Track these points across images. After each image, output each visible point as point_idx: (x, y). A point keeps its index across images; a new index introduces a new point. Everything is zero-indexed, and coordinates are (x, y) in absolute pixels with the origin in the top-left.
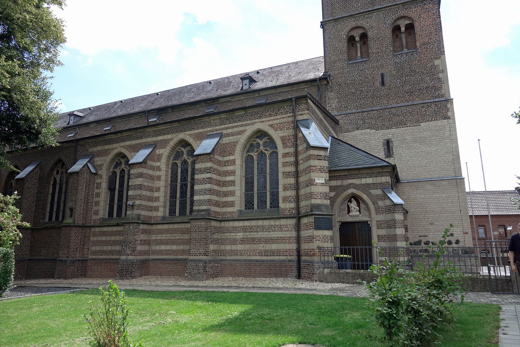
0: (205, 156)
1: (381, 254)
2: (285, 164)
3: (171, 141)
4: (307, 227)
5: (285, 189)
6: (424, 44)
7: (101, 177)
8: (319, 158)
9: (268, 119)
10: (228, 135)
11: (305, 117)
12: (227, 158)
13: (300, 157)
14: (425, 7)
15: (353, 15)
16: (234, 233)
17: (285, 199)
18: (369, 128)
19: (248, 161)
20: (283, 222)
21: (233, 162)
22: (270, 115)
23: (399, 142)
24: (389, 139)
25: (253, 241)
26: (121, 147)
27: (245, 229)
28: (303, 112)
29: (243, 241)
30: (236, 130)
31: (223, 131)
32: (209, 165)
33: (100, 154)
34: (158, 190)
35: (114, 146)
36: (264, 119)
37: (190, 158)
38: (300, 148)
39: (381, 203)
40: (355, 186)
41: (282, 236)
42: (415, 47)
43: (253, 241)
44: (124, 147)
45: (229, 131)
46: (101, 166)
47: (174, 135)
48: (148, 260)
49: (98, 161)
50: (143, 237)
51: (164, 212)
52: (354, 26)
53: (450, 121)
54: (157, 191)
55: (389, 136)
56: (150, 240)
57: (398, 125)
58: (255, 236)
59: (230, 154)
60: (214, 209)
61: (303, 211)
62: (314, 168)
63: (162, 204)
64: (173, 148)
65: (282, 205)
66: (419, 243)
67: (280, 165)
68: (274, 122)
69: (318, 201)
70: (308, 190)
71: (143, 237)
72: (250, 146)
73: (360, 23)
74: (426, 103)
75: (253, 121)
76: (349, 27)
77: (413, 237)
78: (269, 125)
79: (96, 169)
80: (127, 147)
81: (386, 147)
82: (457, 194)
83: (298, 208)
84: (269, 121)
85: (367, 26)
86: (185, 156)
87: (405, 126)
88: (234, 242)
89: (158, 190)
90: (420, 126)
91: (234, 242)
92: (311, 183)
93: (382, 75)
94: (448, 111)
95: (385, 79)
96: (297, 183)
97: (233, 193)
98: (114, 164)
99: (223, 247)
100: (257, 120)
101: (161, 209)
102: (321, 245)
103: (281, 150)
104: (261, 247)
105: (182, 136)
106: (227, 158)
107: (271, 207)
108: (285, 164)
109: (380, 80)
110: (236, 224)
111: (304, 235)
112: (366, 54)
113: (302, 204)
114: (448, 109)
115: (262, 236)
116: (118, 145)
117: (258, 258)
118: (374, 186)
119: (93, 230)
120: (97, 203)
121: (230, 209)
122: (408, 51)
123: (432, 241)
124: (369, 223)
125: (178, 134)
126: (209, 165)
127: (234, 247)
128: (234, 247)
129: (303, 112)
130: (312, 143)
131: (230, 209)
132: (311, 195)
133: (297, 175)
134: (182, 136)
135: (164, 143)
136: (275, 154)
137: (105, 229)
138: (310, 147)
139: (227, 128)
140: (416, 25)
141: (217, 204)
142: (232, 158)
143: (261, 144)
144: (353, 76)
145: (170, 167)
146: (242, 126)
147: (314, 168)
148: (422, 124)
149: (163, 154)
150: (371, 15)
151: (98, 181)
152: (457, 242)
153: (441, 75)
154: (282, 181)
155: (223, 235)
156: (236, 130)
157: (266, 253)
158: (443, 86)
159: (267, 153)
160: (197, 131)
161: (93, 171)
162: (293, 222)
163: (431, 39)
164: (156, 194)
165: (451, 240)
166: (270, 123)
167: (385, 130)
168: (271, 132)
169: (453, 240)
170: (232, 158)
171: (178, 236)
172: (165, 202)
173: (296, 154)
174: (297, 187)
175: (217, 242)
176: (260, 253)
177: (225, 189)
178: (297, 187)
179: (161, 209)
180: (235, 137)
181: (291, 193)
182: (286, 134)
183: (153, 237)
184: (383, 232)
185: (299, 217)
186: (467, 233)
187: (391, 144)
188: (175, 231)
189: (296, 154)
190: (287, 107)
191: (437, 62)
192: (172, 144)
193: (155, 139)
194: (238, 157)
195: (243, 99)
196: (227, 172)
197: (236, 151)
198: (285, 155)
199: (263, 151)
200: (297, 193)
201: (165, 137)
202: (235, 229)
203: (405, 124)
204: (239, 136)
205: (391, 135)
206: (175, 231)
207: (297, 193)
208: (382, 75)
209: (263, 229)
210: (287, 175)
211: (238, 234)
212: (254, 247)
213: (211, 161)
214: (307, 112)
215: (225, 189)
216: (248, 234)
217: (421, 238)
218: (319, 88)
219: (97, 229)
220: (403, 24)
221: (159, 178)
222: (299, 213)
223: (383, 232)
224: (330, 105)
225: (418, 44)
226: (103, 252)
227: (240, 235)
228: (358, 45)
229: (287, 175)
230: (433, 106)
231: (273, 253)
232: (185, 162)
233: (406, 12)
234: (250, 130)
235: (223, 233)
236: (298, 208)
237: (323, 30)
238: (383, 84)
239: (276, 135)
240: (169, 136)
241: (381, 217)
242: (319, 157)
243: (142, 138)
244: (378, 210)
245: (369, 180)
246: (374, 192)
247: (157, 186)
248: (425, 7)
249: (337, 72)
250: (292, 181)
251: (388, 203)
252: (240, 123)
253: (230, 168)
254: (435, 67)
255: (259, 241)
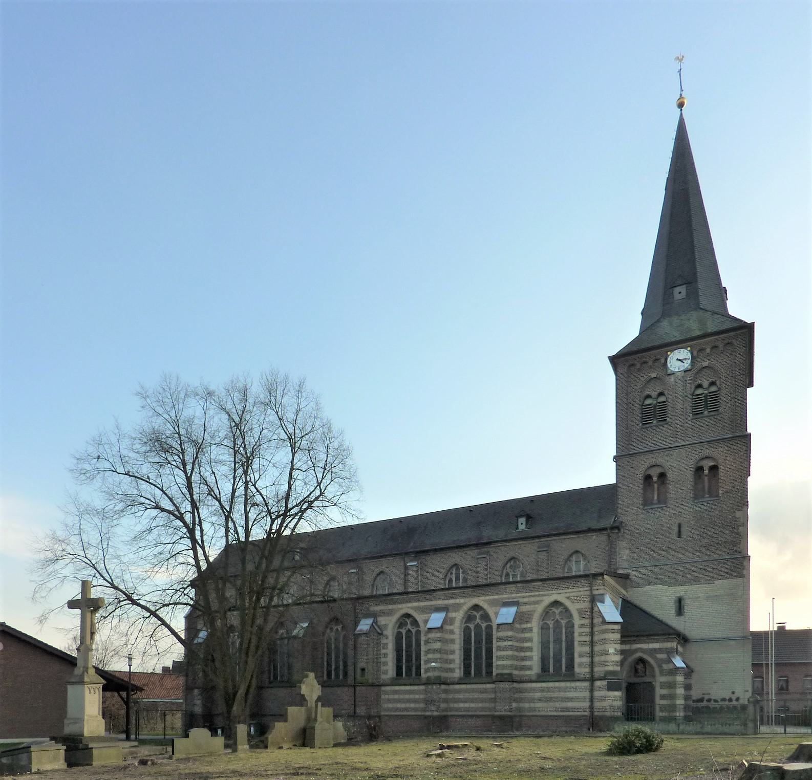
0: (506, 625)
1: (661, 710)
2: (581, 634)
3: (464, 605)
4: (600, 688)
5: (581, 656)
6: (727, 492)
7: (387, 638)
8: (613, 631)
9: (565, 591)
10: (525, 604)
11: (601, 592)
12: (525, 626)
13: (596, 629)
14: (732, 448)
15: (652, 451)
16: (532, 693)
17: (580, 665)
18: (661, 584)
19: (544, 628)
20: (578, 684)
21: (531, 630)
22: (568, 588)
23: (691, 600)
24: (682, 597)
25: (550, 700)
26: (408, 607)
27: (542, 690)
28: (599, 588)
29: (540, 700)
30: (533, 599)
31: (519, 599)
32: (510, 633)
33: (383, 613)
34: (453, 652)
35: (400, 606)
36: (561, 591)
37: (483, 622)
38: (595, 621)
39: (665, 666)
40: (641, 650)
41: (577, 695)
42: (717, 496)
43: (550, 700)
44: (412, 608)
45: (526, 600)
46: (386, 625)
47: (467, 600)
48: (447, 716)
49: (382, 620)
50: (443, 696)
51: (460, 673)
52: (651, 464)
53: (745, 580)
54: (451, 654)
55: (682, 594)
56: (448, 699)
57: (690, 582)
58: (552, 696)
59: (527, 622)
60: (516, 672)
61: (596, 675)
62: (608, 640)
63: (458, 666)
64: (466, 613)
65: (577, 669)
66: (701, 700)
67: (576, 634)
68: (571, 594)
69: (611, 668)
70: (603, 658)
71: (443, 696)
72: (546, 613)
73: (659, 461)
74: (723, 559)
75: (551, 592)
76: (647, 465)
77: (695, 694)
78: (566, 597)
79: (380, 629)
80: (415, 609)
81: (678, 604)
82: (743, 654)
83: (592, 671)
84: (566, 593)
85: (667, 465)
86: (478, 620)
87: (699, 583)
88: (532, 700)
89: (453, 652)
90: (713, 583)
91: (532, 700)
92: (605, 653)
93: (680, 526)
94: (744, 569)
95: (682, 530)
96: (592, 651)
97: (530, 658)
98: (399, 623)
99: (522, 705)
100: (554, 592)
101: (457, 671)
102: (611, 703)
103: (577, 621)
104: (558, 705)
105: (475, 601)
106: (525, 626)
107: (566, 671)
108: (581, 634)
109: (676, 529)
110: (534, 685)
111: (597, 695)
112: (663, 500)
113: (596, 669)
114: (744, 567)
115: (559, 695)
116: (404, 605)
117: (555, 714)
118: (660, 651)
119: (383, 688)
120: (385, 664)
121: (528, 672)
122: (709, 499)
123: (714, 698)
124: (653, 683)
125: (471, 599)
126: (510, 633)
127: (532, 705)
128: (532, 705)
129: (599, 588)
130: (608, 619)
131: (528, 672)
132: (604, 664)
133: (592, 643)
134: (475, 601)
135: (457, 607)
136: (570, 626)
137: (397, 688)
138: (605, 622)
139: (524, 597)
140: (721, 468)
141: (516, 668)
142: (529, 625)
143: (557, 613)
144: (648, 523)
145: (462, 630)
146: (539, 596)
147: (608, 640)
148: (716, 582)
149: (455, 618)
150: (672, 452)
151: (384, 641)
152: (737, 699)
153: (741, 529)
154: (578, 649)
155: (521, 694)
156: (533, 599)
157: (563, 710)
158: (742, 541)
159: (563, 622)
160: (492, 597)
161: (379, 631)
162: (587, 684)
163: (735, 486)
164: (451, 657)
165: (732, 697)
166: (568, 595)
167: (678, 587)
168: (568, 603)
169: (734, 698)
170: (529, 625)
171: (476, 696)
172: (460, 664)
173: (592, 625)
174: (592, 655)
175: (516, 700)
176: (557, 710)
177: (523, 654)
178: (592, 655)
179: (457, 671)
180: (532, 606)
181: (587, 660)
182: (582, 607)
183: (451, 696)
184: (665, 692)
185: (592, 680)
186: (747, 691)
187: (682, 603)
188: (473, 691)
189: (592, 625)
190: (584, 582)
191: (738, 514)
192: (465, 608)
193: (446, 602)
194: (535, 625)
195: (521, 544)
196: (525, 638)
197: (534, 620)
198: (582, 626)
199: (559, 620)
200: (592, 660)
201: (457, 601)
202: (534, 690)
203: (699, 581)
204: (537, 606)
205: (684, 593)
206: (473, 691)
207: (592, 660)
208: (680, 526)
209: (560, 689)
210: (582, 643)
211: (537, 694)
212: (551, 704)
213: (512, 630)
214: (602, 587)
215: (523, 654)
216: (546, 694)
217: (703, 696)
218: (609, 537)
219: (388, 688)
220: (707, 464)
221: (453, 641)
222: (592, 676)
223: (665, 692)
224: (620, 556)
225: (720, 492)
226: (397, 709)
227: (538, 695)
228: (656, 486)
229: (582, 643)
230: (729, 563)
231: (568, 709)
232: (478, 627)
233: (711, 452)
234: (548, 600)
235: (521, 693)
236: (592, 671)
237: (616, 464)
238: (679, 534)
239: (573, 608)
240: (462, 601)
241: (663, 679)
242: (613, 631)
243: (431, 600)
244: (662, 672)
245: (656, 646)
246: (660, 656)
247: (452, 649)
248: (732, 448)
249: (630, 518)
250: (587, 649)
251: (671, 666)
252: (537, 593)
253: (527, 635)
254: (735, 519)
255: (557, 699)
